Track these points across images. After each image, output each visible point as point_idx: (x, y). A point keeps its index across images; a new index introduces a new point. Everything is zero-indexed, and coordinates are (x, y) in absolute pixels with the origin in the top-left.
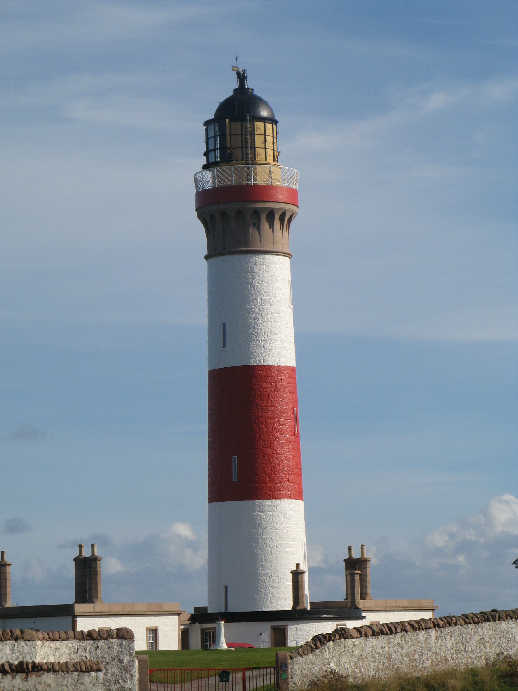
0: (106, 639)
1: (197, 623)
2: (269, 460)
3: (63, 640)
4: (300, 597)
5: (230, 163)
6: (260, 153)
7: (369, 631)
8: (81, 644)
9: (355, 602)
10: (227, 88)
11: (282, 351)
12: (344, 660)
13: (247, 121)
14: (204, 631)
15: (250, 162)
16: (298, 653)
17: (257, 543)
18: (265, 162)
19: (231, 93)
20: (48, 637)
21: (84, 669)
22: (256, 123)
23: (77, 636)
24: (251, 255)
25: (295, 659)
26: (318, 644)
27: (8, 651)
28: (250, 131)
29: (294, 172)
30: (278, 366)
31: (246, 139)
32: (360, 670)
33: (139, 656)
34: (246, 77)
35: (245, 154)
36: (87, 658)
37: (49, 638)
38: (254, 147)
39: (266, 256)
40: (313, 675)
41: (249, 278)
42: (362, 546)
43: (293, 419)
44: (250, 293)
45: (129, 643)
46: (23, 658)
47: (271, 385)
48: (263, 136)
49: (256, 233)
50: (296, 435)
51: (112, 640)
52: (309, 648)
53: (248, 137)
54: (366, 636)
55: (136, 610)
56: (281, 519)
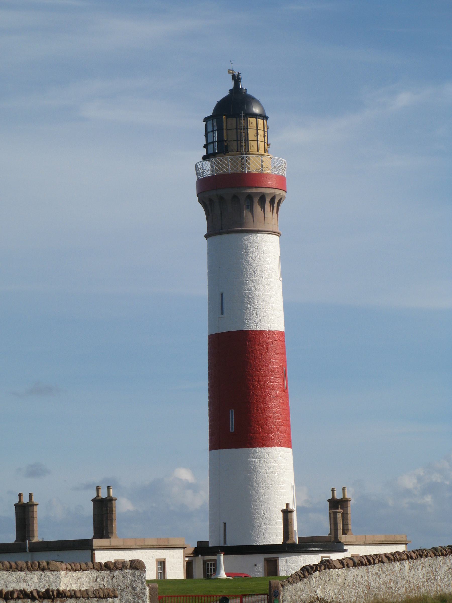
0: (121, 569)
1: (200, 556)
2: (262, 413)
3: (83, 570)
4: (290, 533)
5: (227, 154)
6: (253, 144)
7: (351, 562)
8: (99, 574)
9: (338, 537)
10: (223, 89)
11: (273, 318)
12: (328, 587)
13: (241, 117)
14: (206, 562)
15: (244, 153)
16: (289, 582)
17: (252, 486)
18: (258, 153)
19: (227, 93)
20: (70, 567)
21: (102, 596)
22: (249, 119)
23: (95, 567)
24: (245, 234)
25: (286, 587)
26: (306, 574)
27: (36, 580)
28: (244, 126)
29: (283, 161)
30: (269, 331)
31: (241, 133)
32: (343, 596)
33: (150, 584)
34: (240, 79)
35: (239, 146)
36: (104, 586)
37: (72, 568)
38: (248, 140)
39: (258, 235)
40: (302, 600)
41: (244, 254)
42: (344, 487)
43: (283, 377)
44: (244, 267)
45: (141, 573)
46: (49, 586)
47: (263, 347)
48: (256, 130)
49: (250, 214)
50: (285, 391)
51: (126, 571)
52: (298, 577)
53: (243, 131)
54: (348, 567)
55: (146, 544)
56: (272, 464)
